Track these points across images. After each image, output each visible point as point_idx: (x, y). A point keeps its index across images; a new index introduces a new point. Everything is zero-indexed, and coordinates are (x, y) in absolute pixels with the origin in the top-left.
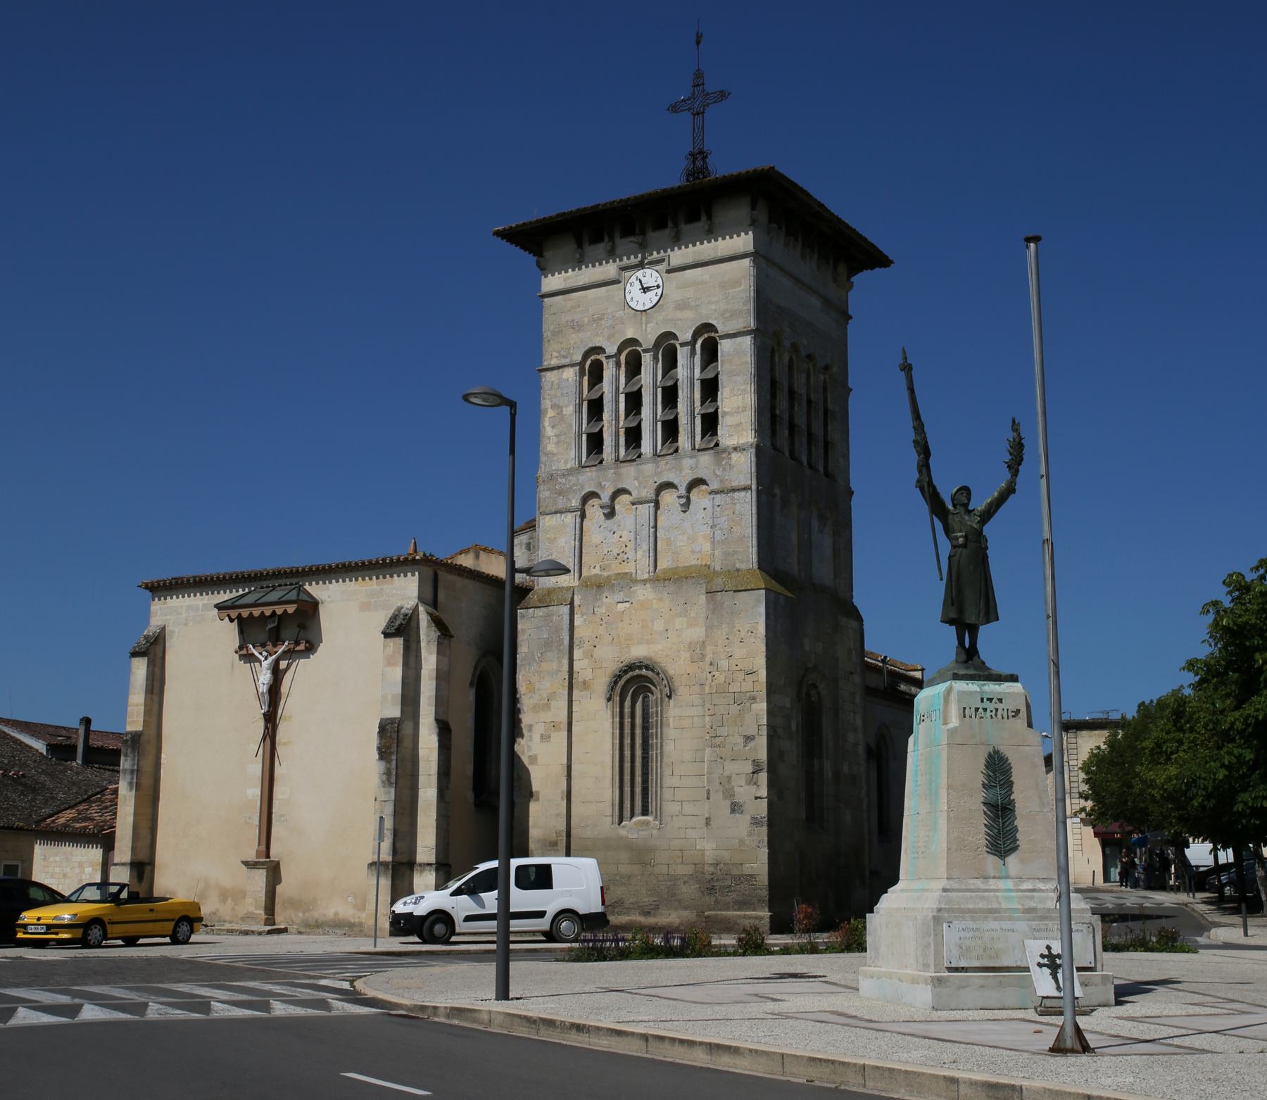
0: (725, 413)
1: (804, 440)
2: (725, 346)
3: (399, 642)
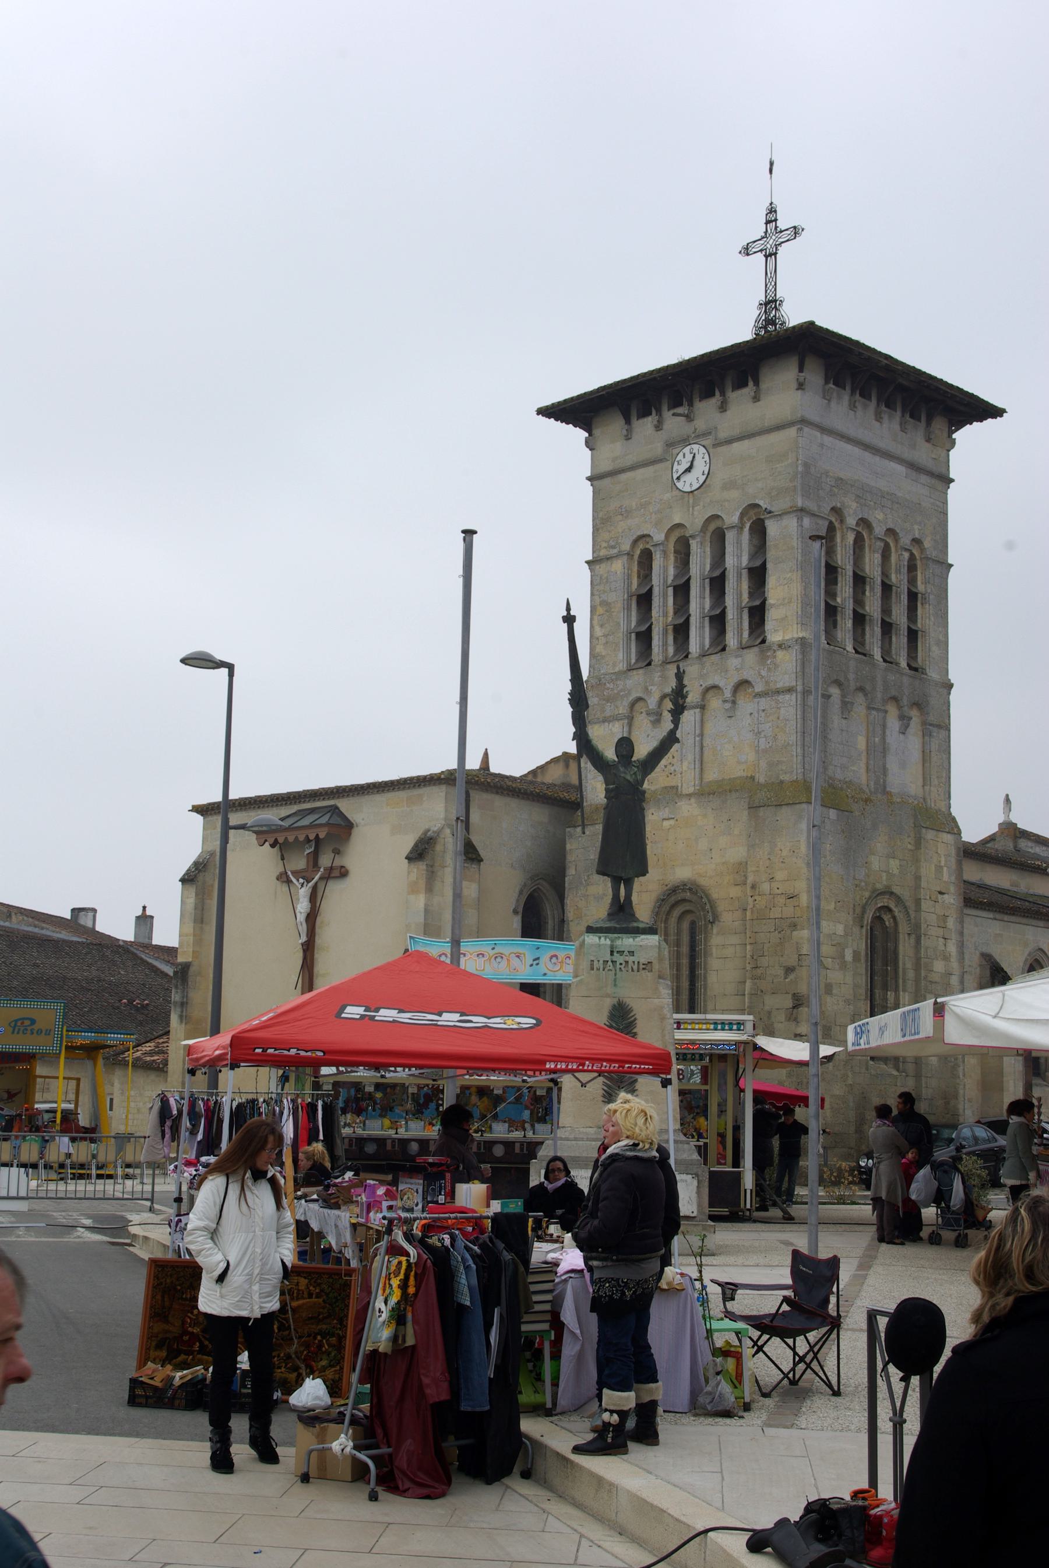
0: (772, 606)
1: (878, 630)
2: (772, 528)
3: (422, 866)
